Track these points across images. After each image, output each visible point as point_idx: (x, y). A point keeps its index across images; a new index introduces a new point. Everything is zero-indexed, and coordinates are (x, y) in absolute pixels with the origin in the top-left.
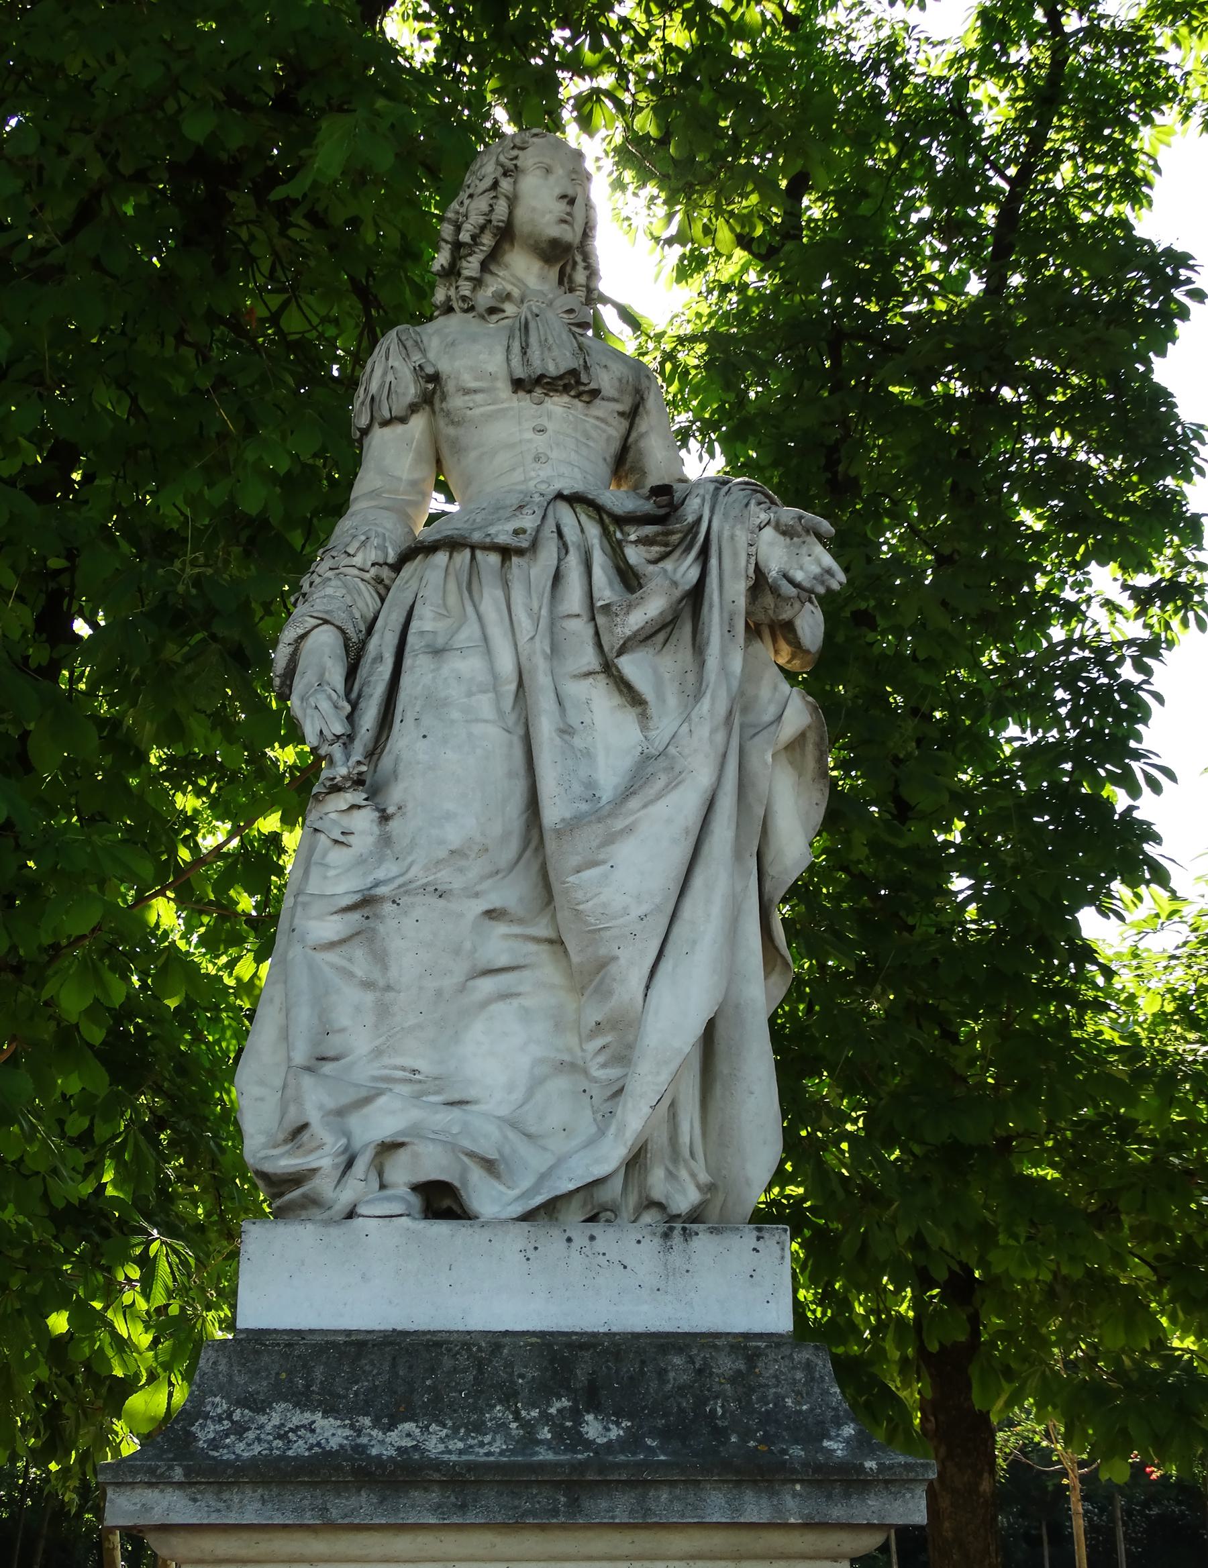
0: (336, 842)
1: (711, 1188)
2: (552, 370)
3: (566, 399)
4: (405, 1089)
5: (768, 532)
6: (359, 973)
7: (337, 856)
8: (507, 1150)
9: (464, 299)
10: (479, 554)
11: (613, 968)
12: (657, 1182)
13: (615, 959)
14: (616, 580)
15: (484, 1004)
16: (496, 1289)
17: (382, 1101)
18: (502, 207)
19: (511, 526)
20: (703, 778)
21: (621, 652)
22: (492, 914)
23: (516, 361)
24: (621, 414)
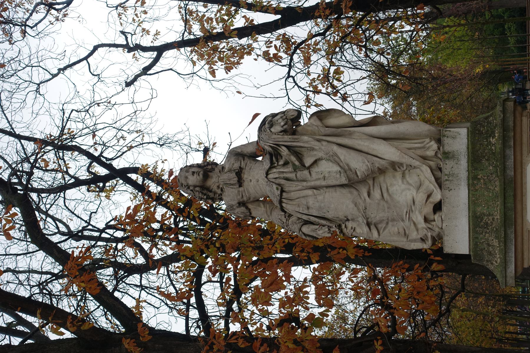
2: (236, 179)
3: (242, 175)
4: (411, 214)
5: (272, 130)
6: (384, 226)
7: (358, 230)
8: (425, 191)
11: (380, 167)
12: (430, 153)
14: (286, 166)
15: (389, 195)
16: (460, 197)
17: (414, 220)
18: (197, 189)
19: (276, 191)
20: (335, 148)
22: (369, 195)
23: (235, 187)
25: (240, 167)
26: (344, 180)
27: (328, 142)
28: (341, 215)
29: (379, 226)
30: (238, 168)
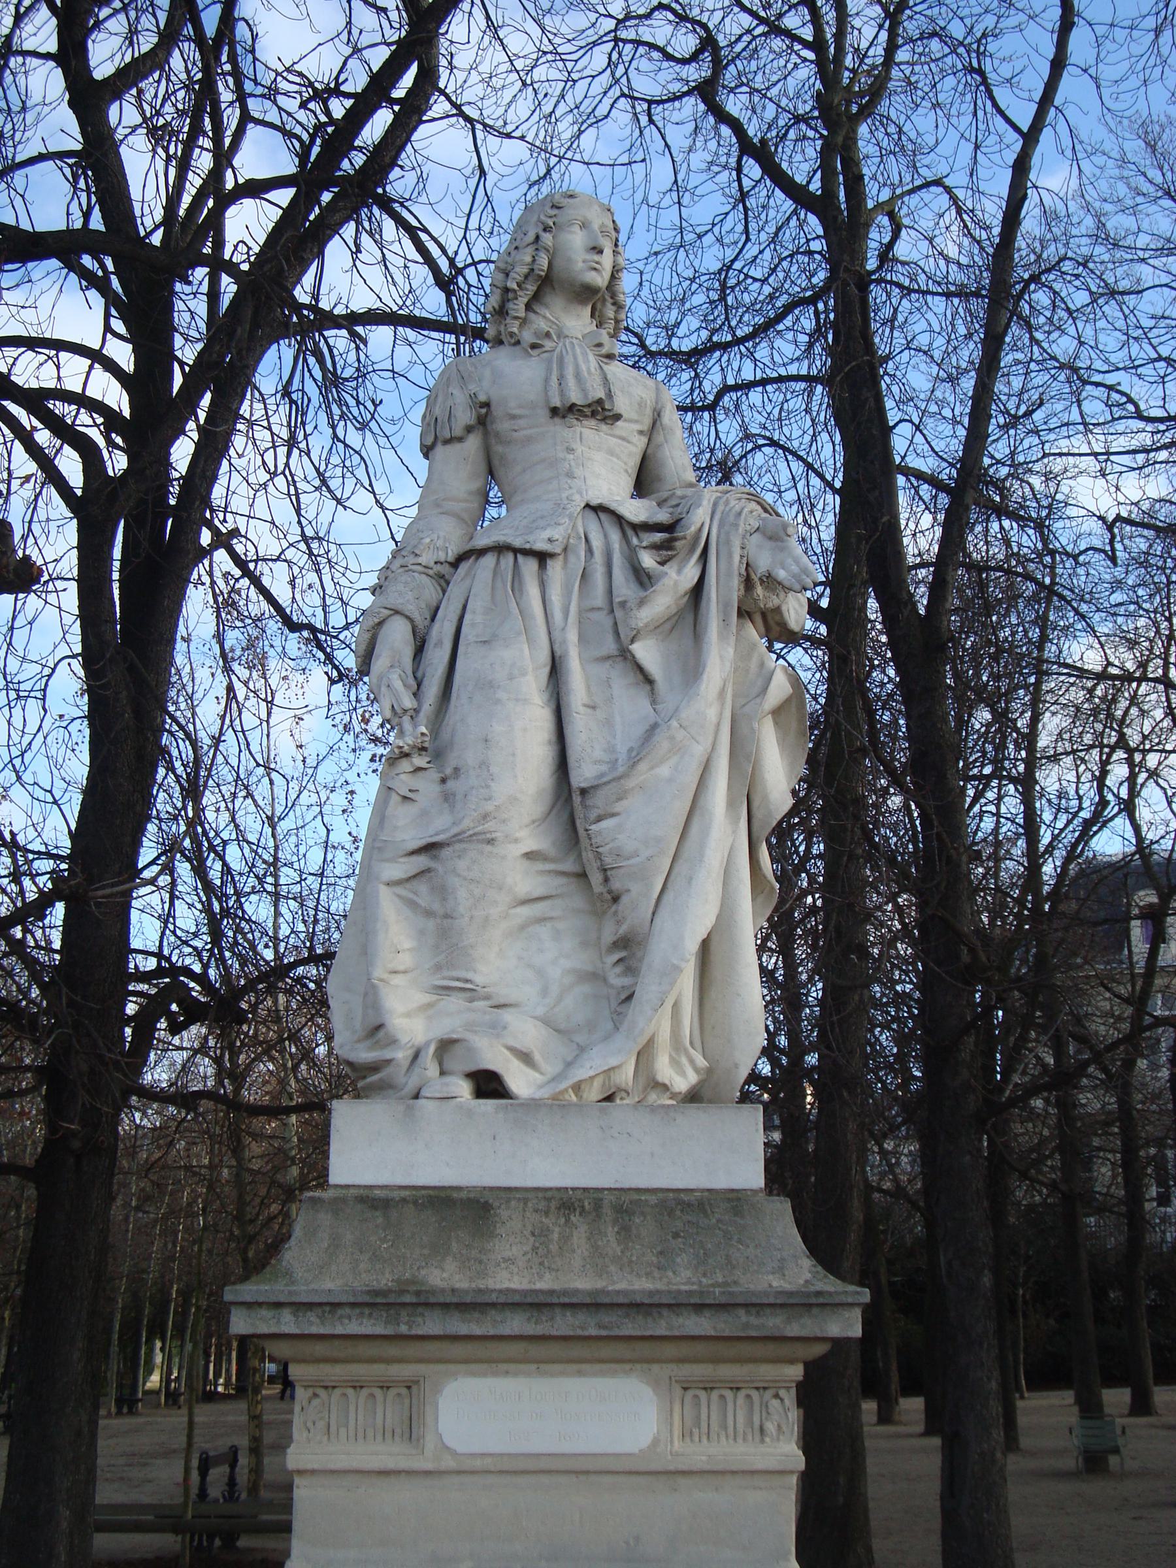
0: (405, 798)
1: (710, 1071)
9: (512, 334)
10: (520, 558)
13: (628, 891)
14: (632, 578)
19: (546, 534)
20: (699, 751)
21: (632, 641)
24: (641, 432)
25: (618, 417)
26: (583, 773)
28: (466, 754)
29: (422, 887)
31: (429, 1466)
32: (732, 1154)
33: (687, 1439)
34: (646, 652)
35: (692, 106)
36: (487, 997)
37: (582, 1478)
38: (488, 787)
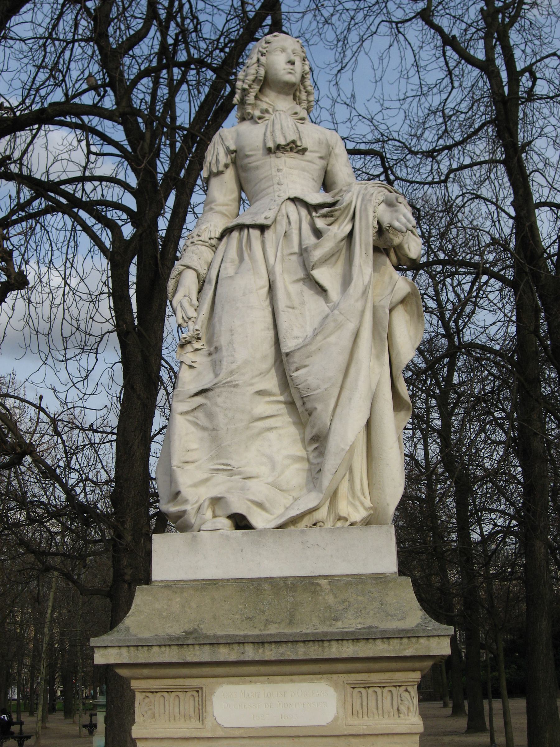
1: (374, 509)
4: (226, 473)
10: (251, 230)
15: (260, 433)
20: (351, 326)
22: (260, 393)
24: (321, 158)
26: (288, 345)
27: (363, 312)
29: (200, 414)
30: (304, 146)
31: (210, 735)
32: (381, 554)
33: (355, 717)
34: (322, 275)
35: (419, 23)
36: (239, 474)
37: (296, 740)
38: (233, 356)
